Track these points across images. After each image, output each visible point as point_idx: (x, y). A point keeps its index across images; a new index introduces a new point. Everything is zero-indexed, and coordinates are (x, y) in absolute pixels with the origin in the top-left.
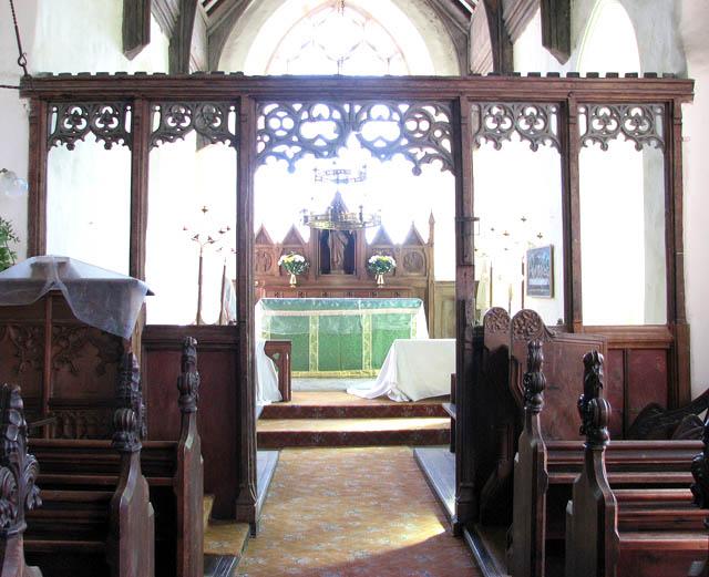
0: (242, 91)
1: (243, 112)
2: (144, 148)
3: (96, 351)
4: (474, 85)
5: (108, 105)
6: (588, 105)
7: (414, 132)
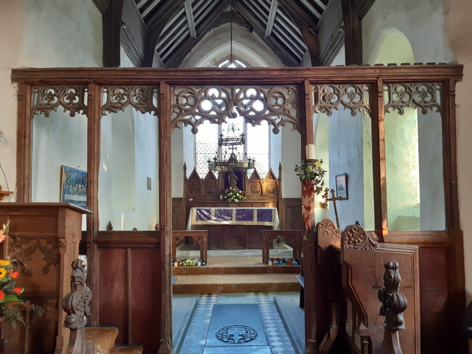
0: (160, 79)
1: (161, 92)
2: (97, 116)
3: (43, 256)
4: (314, 73)
5: (51, 88)
6: (391, 85)
7: (274, 106)
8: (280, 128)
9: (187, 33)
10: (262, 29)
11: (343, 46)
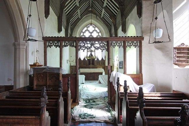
8: (103, 51)
9: (78, 17)
10: (100, 16)
11: (120, 26)
